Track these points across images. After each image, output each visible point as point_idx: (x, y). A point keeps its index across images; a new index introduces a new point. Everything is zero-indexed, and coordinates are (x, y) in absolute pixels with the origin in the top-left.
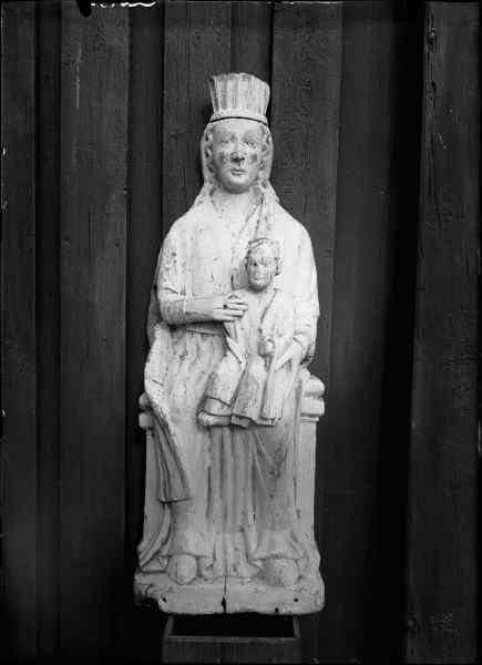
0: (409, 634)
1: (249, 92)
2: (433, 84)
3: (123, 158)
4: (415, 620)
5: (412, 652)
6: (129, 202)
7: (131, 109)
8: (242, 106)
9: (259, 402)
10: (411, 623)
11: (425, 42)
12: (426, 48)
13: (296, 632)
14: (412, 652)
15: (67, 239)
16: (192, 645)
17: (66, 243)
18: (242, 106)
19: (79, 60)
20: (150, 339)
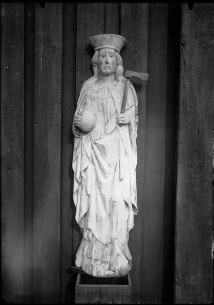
0: (176, 284)
1: (100, 114)
2: (184, 61)
3: (60, 91)
4: (179, 279)
5: (178, 292)
6: (62, 108)
7: (63, 46)
8: (109, 47)
9: (125, 143)
10: (177, 280)
11: (181, 44)
12: (181, 47)
13: (130, 282)
14: (178, 292)
15: (36, 123)
16: (88, 287)
17: (37, 125)
18: (109, 47)
19: (42, 51)
20: (77, 97)
